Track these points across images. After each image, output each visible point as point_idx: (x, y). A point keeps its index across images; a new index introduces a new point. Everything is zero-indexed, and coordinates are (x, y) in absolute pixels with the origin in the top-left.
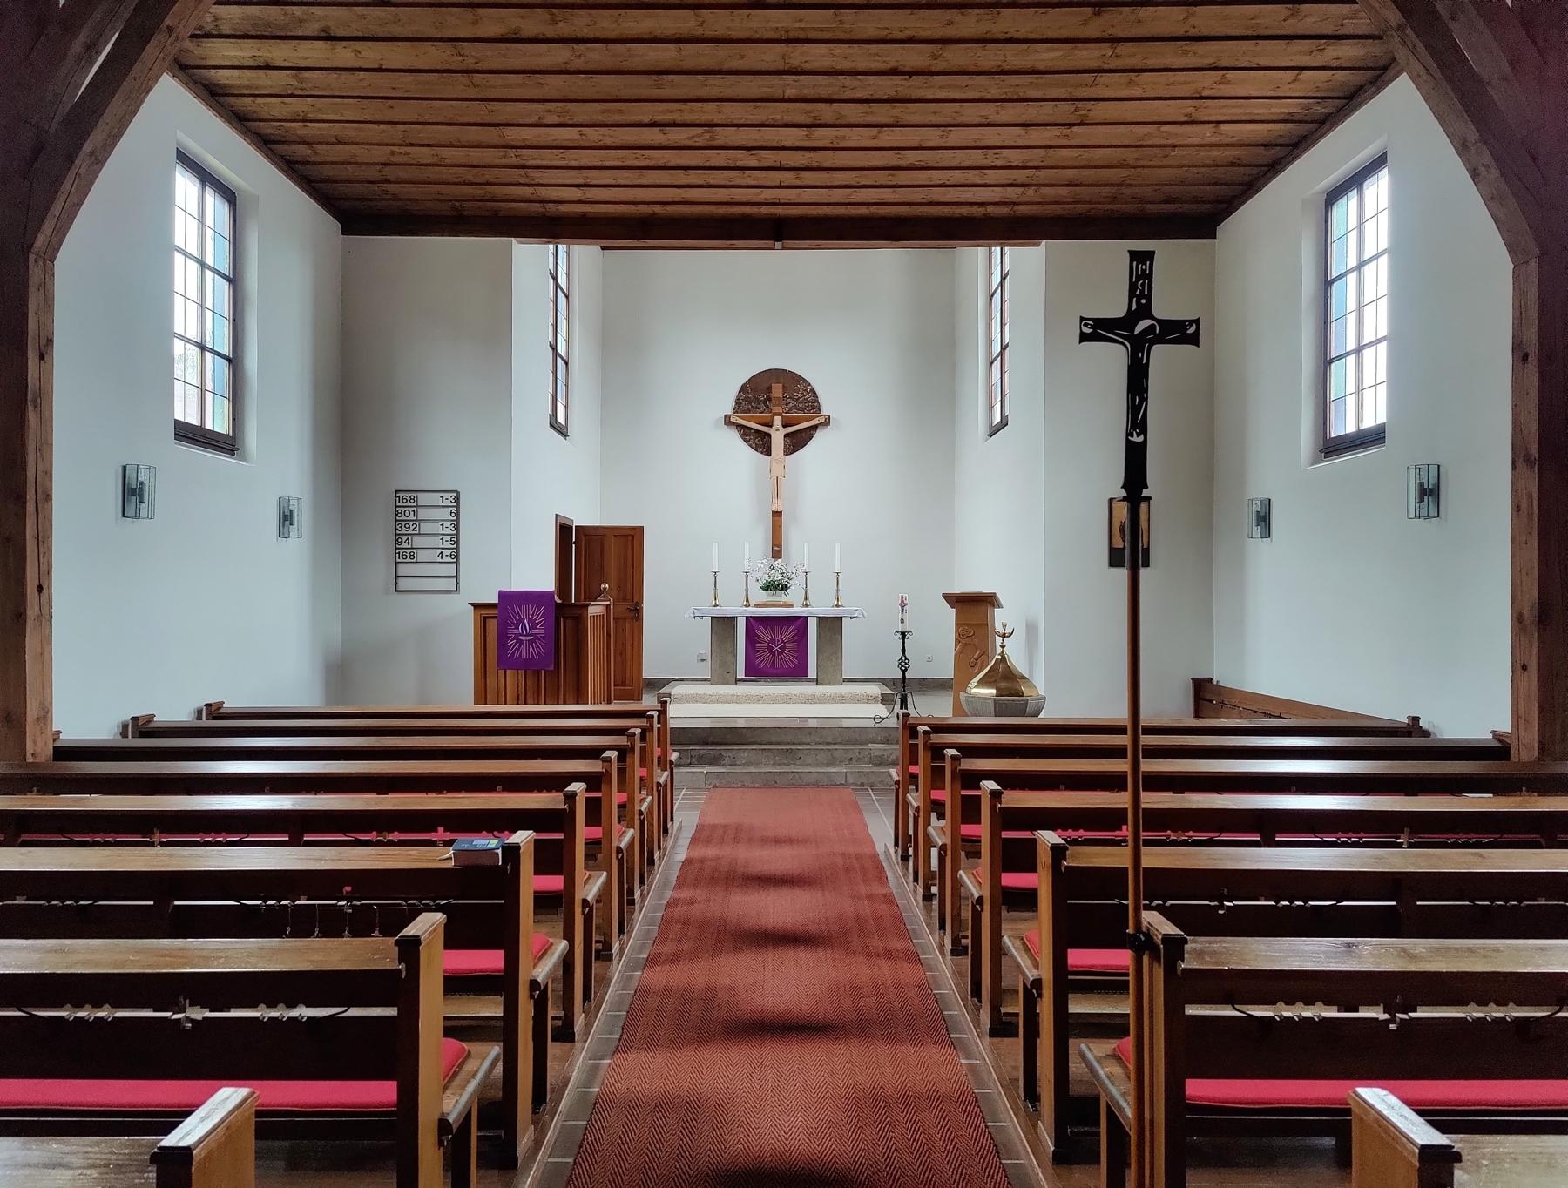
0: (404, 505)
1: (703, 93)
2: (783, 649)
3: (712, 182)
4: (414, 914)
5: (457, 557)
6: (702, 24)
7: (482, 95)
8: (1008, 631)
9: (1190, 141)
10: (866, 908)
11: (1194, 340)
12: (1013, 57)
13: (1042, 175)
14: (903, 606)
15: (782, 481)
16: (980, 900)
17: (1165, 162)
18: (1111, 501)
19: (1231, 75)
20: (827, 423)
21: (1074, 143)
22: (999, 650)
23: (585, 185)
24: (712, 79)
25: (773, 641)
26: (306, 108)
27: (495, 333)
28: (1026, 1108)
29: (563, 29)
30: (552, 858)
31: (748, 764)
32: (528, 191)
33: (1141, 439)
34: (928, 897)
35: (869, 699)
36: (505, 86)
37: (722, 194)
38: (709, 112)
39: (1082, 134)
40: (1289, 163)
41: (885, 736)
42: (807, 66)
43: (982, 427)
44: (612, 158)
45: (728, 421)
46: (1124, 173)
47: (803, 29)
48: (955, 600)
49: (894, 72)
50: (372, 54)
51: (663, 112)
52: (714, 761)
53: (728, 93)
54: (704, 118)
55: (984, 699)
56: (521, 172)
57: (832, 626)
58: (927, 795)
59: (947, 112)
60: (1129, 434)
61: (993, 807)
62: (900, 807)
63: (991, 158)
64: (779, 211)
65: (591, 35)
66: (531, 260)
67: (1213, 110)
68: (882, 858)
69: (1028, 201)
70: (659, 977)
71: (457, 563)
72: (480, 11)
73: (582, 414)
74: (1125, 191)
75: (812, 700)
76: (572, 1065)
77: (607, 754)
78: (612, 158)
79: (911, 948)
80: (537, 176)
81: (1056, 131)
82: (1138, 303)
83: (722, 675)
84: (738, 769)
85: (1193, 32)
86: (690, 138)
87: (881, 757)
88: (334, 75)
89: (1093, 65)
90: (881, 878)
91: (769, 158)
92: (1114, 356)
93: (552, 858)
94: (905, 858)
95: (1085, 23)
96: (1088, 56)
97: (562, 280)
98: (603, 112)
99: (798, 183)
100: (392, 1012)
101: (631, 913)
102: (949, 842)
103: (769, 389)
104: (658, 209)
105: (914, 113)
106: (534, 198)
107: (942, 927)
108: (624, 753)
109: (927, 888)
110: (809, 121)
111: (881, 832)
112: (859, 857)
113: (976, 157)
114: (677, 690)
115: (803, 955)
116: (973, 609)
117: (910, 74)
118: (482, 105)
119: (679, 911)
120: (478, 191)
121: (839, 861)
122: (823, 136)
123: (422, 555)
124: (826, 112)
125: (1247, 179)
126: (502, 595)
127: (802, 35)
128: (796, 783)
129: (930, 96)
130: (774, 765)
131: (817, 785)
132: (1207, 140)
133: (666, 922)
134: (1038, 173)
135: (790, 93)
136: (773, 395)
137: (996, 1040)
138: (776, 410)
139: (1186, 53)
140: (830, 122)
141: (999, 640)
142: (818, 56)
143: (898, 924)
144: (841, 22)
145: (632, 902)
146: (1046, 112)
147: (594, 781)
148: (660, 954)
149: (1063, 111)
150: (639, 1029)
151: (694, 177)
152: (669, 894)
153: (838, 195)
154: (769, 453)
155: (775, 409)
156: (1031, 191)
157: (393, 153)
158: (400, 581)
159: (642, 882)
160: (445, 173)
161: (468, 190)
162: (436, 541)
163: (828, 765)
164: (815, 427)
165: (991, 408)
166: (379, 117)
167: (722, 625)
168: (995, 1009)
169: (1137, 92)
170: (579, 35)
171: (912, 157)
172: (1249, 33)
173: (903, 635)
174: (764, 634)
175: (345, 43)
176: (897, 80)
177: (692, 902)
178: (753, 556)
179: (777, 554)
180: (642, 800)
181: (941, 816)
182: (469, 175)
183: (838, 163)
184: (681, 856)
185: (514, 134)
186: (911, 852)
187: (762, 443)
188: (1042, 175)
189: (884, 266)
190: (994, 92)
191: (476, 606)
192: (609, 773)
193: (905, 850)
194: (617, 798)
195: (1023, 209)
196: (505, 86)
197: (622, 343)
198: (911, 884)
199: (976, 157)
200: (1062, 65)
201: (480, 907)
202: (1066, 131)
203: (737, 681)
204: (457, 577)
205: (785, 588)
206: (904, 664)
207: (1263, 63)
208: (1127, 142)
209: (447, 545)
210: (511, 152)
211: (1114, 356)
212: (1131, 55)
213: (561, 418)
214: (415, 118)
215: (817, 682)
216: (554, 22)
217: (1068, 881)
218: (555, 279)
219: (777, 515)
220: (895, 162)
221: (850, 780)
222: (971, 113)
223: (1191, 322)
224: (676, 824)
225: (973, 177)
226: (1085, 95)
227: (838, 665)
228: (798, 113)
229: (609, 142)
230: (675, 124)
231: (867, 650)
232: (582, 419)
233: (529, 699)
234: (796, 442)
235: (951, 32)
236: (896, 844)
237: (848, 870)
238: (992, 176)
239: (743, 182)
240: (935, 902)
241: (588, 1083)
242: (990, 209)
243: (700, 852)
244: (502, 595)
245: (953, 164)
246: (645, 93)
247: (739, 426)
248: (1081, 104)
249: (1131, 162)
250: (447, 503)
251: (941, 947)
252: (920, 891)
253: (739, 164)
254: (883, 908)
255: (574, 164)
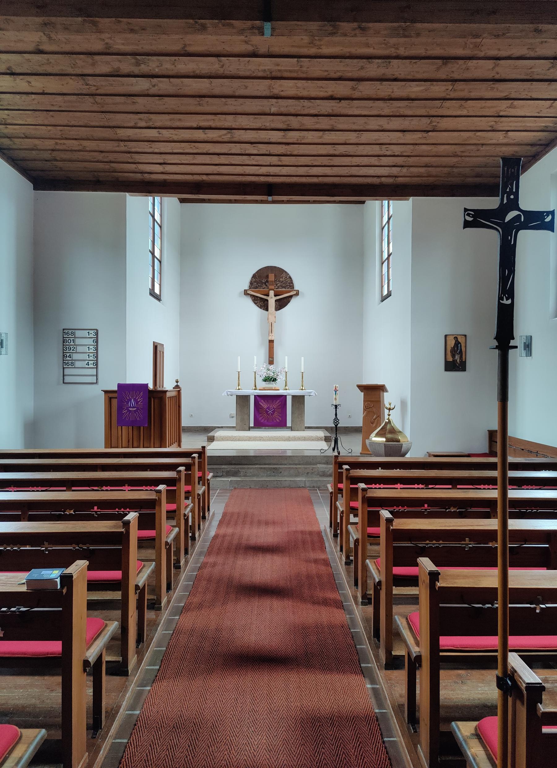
0: (67, 337)
1: (225, 109)
2: (274, 412)
3: (233, 162)
4: (126, 515)
5: (97, 365)
6: (223, 66)
7: (102, 109)
8: (392, 407)
9: (490, 142)
10: (313, 568)
11: (550, 227)
12: (397, 89)
13: (412, 160)
14: (336, 391)
15: (274, 325)
16: (380, 583)
17: (478, 154)
18: (446, 336)
19: (516, 102)
20: (297, 294)
21: (428, 142)
22: (386, 417)
23: (165, 164)
24: (229, 101)
25: (268, 408)
26: (5, 117)
27: (116, 245)
28: (409, 729)
29: (144, 69)
30: (172, 496)
31: (254, 476)
32: (134, 166)
33: (509, 302)
34: (348, 563)
35: (318, 439)
36: (114, 104)
37: (239, 170)
38: (229, 121)
39: (433, 137)
40: (544, 154)
41: (325, 460)
42: (283, 94)
43: (378, 297)
44: (177, 148)
45: (246, 293)
46: (455, 160)
47: (279, 71)
48: (362, 388)
49: (331, 98)
50: (38, 84)
51: (204, 120)
52: (235, 474)
53: (239, 109)
54: (227, 124)
55: (379, 444)
56: (129, 155)
57: (299, 400)
58: (347, 504)
59: (360, 123)
60: (500, 298)
61: (388, 529)
62: (333, 509)
63: (384, 150)
64: (270, 179)
65: (160, 73)
66: (140, 209)
67: (505, 124)
68: (323, 534)
69: (404, 175)
70: (188, 621)
71: (97, 368)
72: (97, 58)
73: (169, 288)
74: (455, 170)
75: (289, 439)
76: (124, 696)
77: (194, 455)
78: (177, 148)
79: (338, 597)
80: (137, 158)
81: (419, 135)
82: (508, 198)
83: (242, 426)
84: (247, 479)
85: (497, 77)
86: (220, 136)
87: (324, 472)
88: (18, 96)
89: (442, 95)
90: (323, 548)
91: (263, 149)
92: (490, 238)
93: (172, 496)
94: (335, 536)
95: (438, 69)
96: (438, 89)
97: (157, 217)
98: (171, 120)
99: (280, 163)
100: (61, 609)
101: (177, 575)
102: (360, 537)
103: (267, 277)
104: (205, 178)
105: (342, 123)
106: (137, 170)
107: (356, 584)
108: (188, 467)
109: (347, 557)
110: (285, 127)
111: (322, 517)
112: (311, 533)
113: (376, 150)
114: (218, 434)
115: (276, 603)
116: (373, 393)
117: (340, 99)
118: (103, 115)
119: (206, 571)
120: (107, 166)
121: (300, 536)
122: (293, 136)
123: (78, 364)
124: (294, 122)
125: (529, 154)
126: (120, 386)
127: (279, 74)
128: (278, 487)
129: (350, 113)
130: (267, 476)
131: (290, 487)
132: (501, 141)
133: (197, 579)
134: (409, 159)
135: (274, 110)
136: (270, 279)
137: (389, 672)
138: (271, 288)
139: (492, 89)
140: (296, 127)
141: (386, 412)
142: (288, 87)
143: (332, 583)
144: (301, 67)
145: (178, 567)
146: (414, 123)
147: (188, 467)
148: (191, 604)
149: (424, 123)
150: (169, 666)
151: (223, 160)
152: (202, 559)
153: (302, 171)
154: (267, 309)
155: (271, 287)
156: (405, 170)
157: (56, 144)
158: (66, 377)
159: (186, 552)
160: (87, 156)
161: (101, 166)
162: (85, 357)
163: (296, 476)
164: (291, 297)
165: (382, 287)
166: (46, 122)
167: (242, 400)
168: (388, 651)
169: (465, 113)
170: (154, 72)
171: (341, 149)
172: (528, 77)
173: (336, 407)
174: (264, 405)
175: (21, 77)
176: (333, 103)
177: (214, 565)
178: (258, 363)
179: (271, 362)
180: (187, 507)
181: (356, 515)
182: (100, 157)
183: (301, 152)
184: (212, 533)
185: (122, 133)
186: (339, 532)
187: (263, 304)
188: (412, 160)
189: (327, 214)
190: (386, 112)
191: (106, 392)
192: (194, 463)
193: (335, 531)
194: (197, 474)
195: (400, 180)
196: (114, 104)
197: (190, 250)
198: (339, 553)
199: (376, 150)
200: (424, 95)
201: (108, 552)
202: (425, 134)
203: (250, 428)
204: (97, 375)
205: (275, 380)
206: (336, 420)
207: (534, 96)
208: (456, 142)
209: (91, 358)
210: (122, 144)
211: (490, 238)
212: (463, 90)
213: (157, 291)
214: (66, 122)
215: (291, 429)
216: (138, 64)
217: (438, 595)
218: (153, 216)
219: (271, 342)
220: (331, 152)
221: (307, 485)
222: (373, 123)
223: (548, 213)
224: (211, 513)
225: (374, 161)
226: (435, 114)
227: (303, 421)
228: (278, 121)
229: (175, 138)
230: (211, 128)
231: (316, 412)
232: (169, 293)
233: (135, 444)
234: (281, 304)
235: (362, 74)
236: (331, 526)
237: (304, 542)
238: (385, 161)
239: (250, 163)
240: (352, 566)
241: (132, 707)
242: (383, 179)
243: (222, 531)
244: (120, 386)
245: (365, 153)
246: (192, 109)
247: (252, 296)
248: (434, 119)
249: (459, 154)
250: (91, 336)
251: (355, 598)
252: (344, 558)
253: (247, 152)
254: (323, 568)
255: (156, 151)
